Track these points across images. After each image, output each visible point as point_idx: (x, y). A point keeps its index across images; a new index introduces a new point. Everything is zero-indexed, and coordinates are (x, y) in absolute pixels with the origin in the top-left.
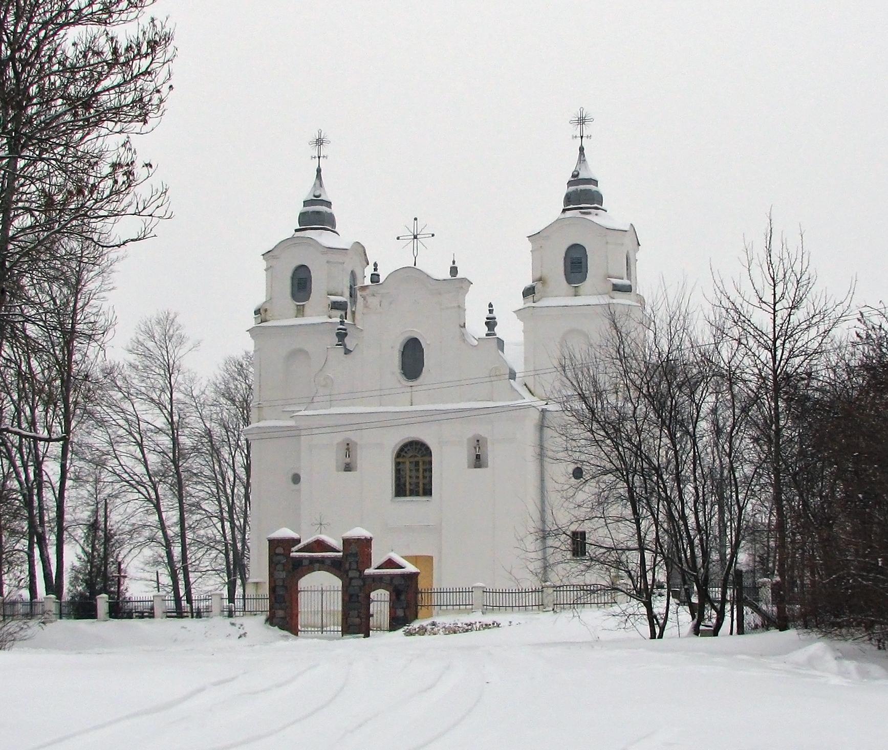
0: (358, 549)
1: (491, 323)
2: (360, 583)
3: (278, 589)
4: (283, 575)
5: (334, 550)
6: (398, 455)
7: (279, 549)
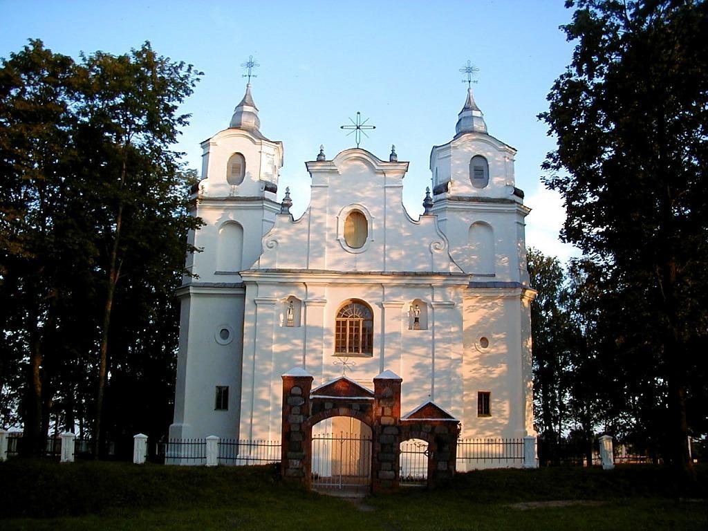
2: (395, 431)
3: (292, 434)
6: (339, 315)
7: (297, 388)
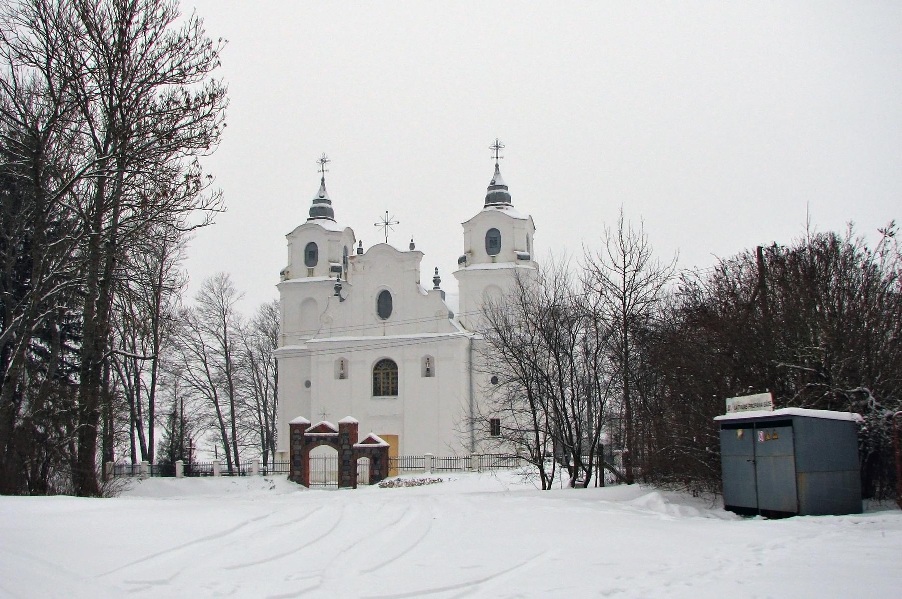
0: (349, 431)
1: (437, 281)
2: (350, 453)
4: (299, 447)
5: (333, 431)
6: (376, 368)
7: (297, 430)
